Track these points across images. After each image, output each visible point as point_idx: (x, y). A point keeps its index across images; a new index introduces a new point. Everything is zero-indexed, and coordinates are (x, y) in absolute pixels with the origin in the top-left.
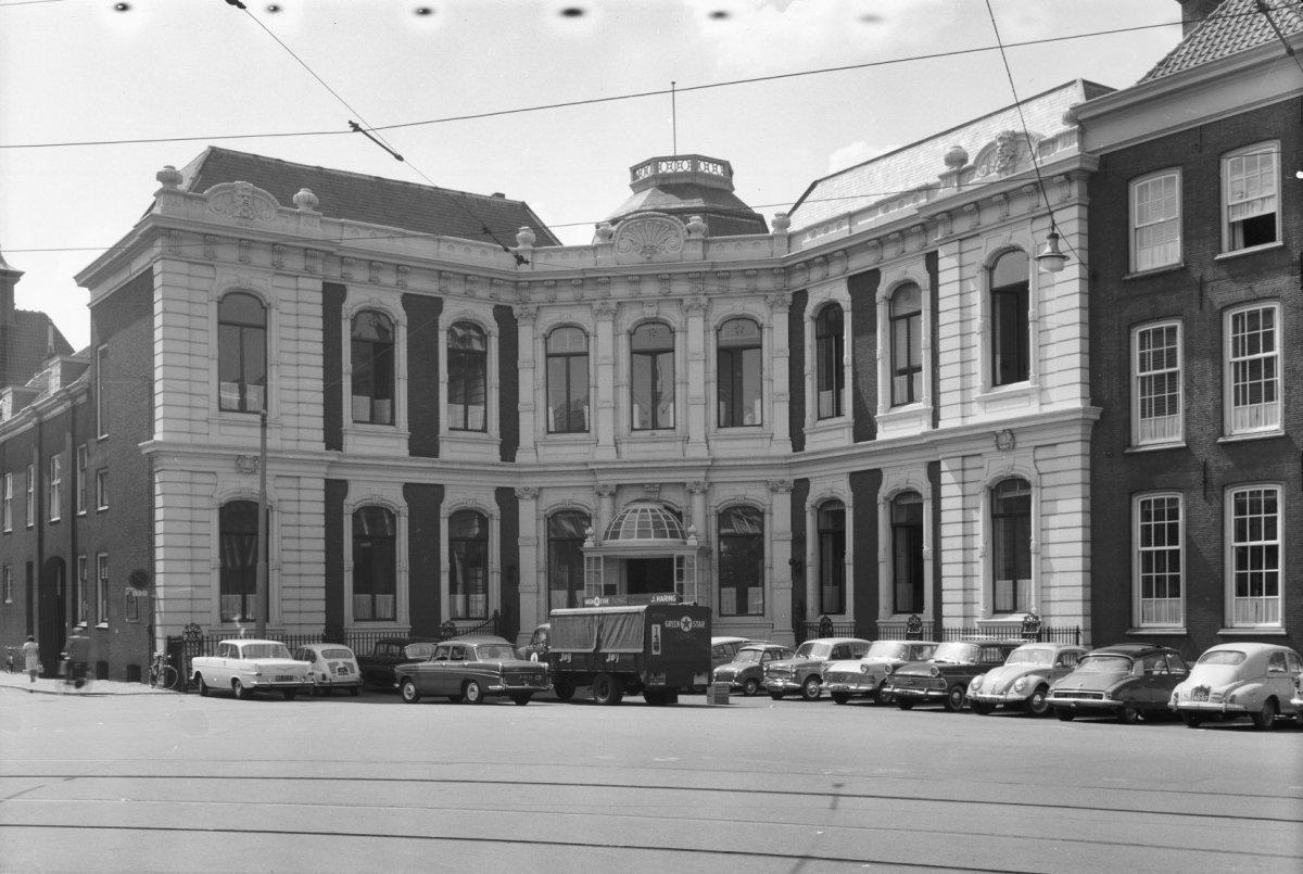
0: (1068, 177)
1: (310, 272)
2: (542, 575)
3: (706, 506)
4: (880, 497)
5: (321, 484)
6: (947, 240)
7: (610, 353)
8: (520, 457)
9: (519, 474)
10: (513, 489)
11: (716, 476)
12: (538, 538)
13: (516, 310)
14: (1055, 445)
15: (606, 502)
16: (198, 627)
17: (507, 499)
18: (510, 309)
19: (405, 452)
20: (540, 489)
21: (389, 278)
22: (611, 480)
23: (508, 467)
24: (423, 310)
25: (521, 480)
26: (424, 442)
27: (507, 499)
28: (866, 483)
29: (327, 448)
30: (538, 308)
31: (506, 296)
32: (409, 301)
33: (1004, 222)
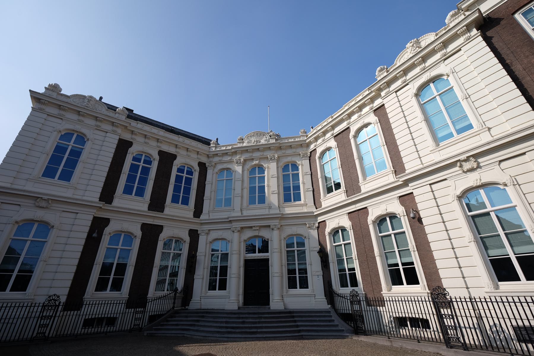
0: (468, 28)
1: (114, 132)
2: (206, 270)
3: (280, 236)
4: (327, 233)
5: (91, 218)
6: (388, 94)
7: (240, 192)
8: (202, 217)
9: (202, 224)
10: (197, 230)
11: (284, 222)
12: (203, 275)
13: (207, 165)
14: (524, 154)
15: (236, 235)
16: (58, 297)
17: (194, 235)
18: (205, 164)
19: (145, 207)
20: (209, 230)
21: (154, 143)
22: (239, 225)
23: (196, 220)
24: (167, 159)
25: (202, 227)
26: (157, 204)
27: (194, 235)
28: (359, 217)
29: (100, 201)
30: (215, 164)
31: (204, 160)
32: (161, 153)
33: (424, 71)
